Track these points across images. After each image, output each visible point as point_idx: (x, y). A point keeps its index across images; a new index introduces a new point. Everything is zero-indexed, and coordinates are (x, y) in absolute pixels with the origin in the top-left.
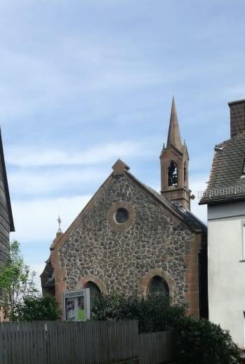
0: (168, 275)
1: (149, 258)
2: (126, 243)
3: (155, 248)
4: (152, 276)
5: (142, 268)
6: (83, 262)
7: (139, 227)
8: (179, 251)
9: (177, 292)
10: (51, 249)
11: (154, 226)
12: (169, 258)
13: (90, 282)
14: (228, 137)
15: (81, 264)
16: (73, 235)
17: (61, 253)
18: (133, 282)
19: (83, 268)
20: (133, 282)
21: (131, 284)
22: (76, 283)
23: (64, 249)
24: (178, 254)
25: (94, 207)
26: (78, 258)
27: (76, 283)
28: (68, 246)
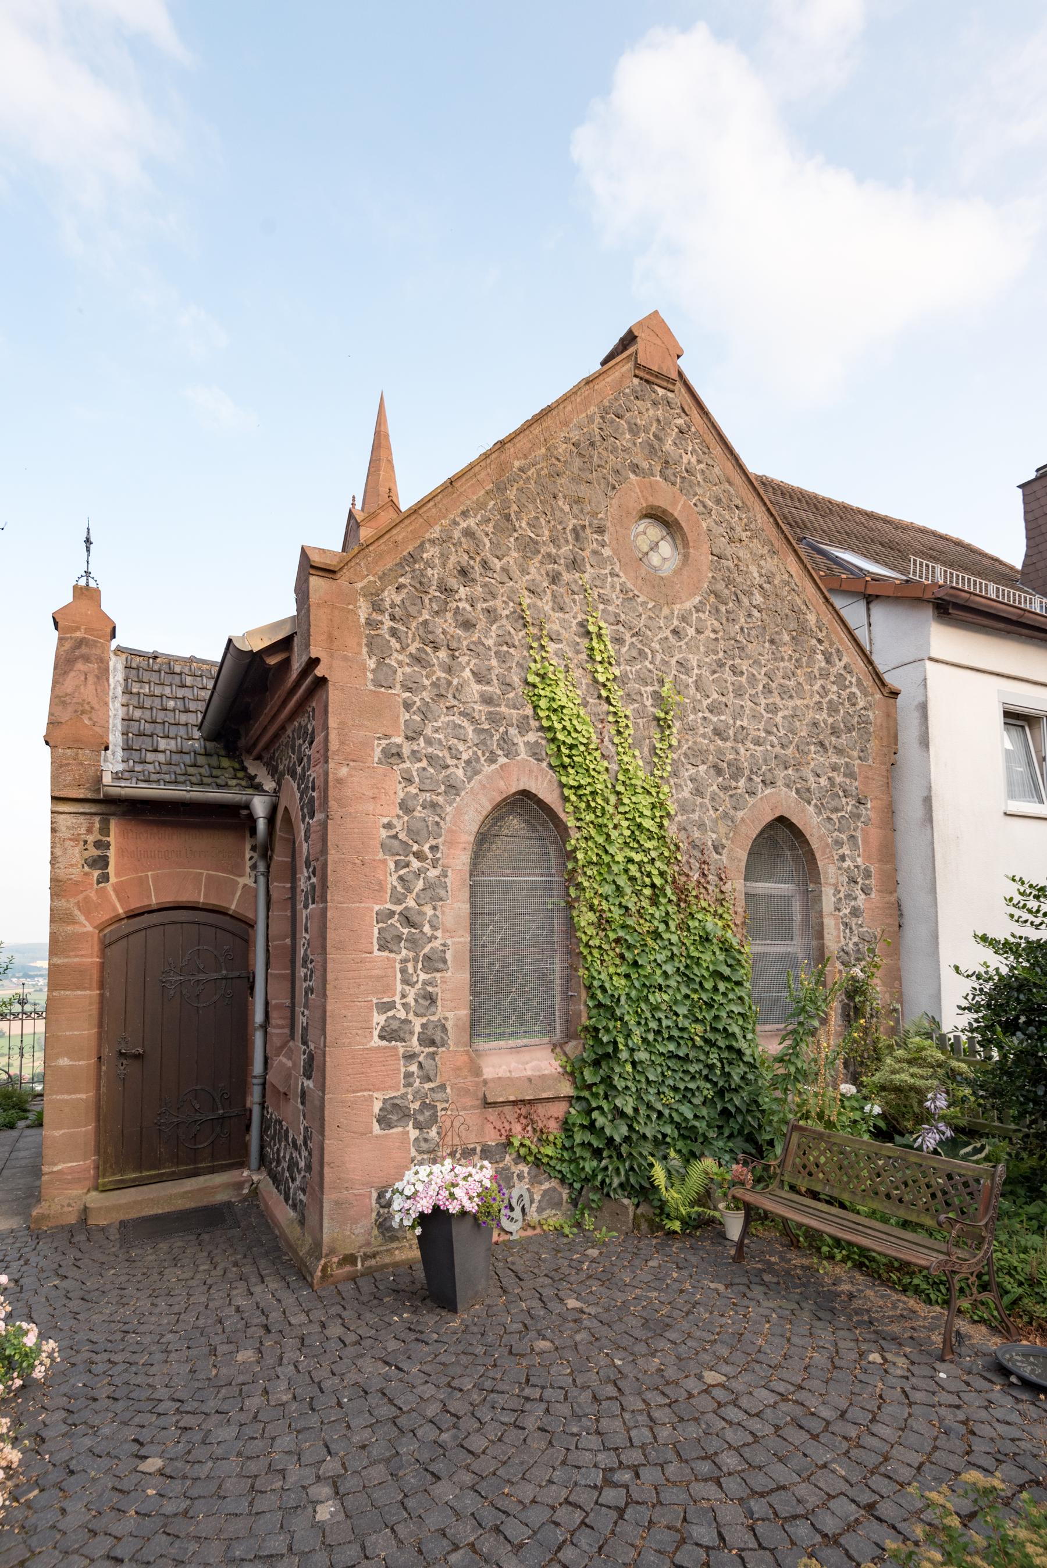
0: (810, 820)
1: (758, 742)
2: (678, 657)
3: (773, 709)
4: (769, 818)
5: (735, 777)
6: (494, 689)
7: (723, 609)
8: (843, 740)
9: (843, 891)
10: (311, 567)
11: (772, 629)
12: (816, 758)
13: (525, 794)
14: (293, 612)
15: (487, 700)
16: (445, 540)
17: (377, 607)
18: (701, 826)
19: (494, 719)
20: (701, 826)
21: (696, 834)
22: (452, 788)
23: (390, 596)
24: (839, 751)
25: (854, 1266)
26: (467, 664)
27: (452, 788)
28: (421, 587)
